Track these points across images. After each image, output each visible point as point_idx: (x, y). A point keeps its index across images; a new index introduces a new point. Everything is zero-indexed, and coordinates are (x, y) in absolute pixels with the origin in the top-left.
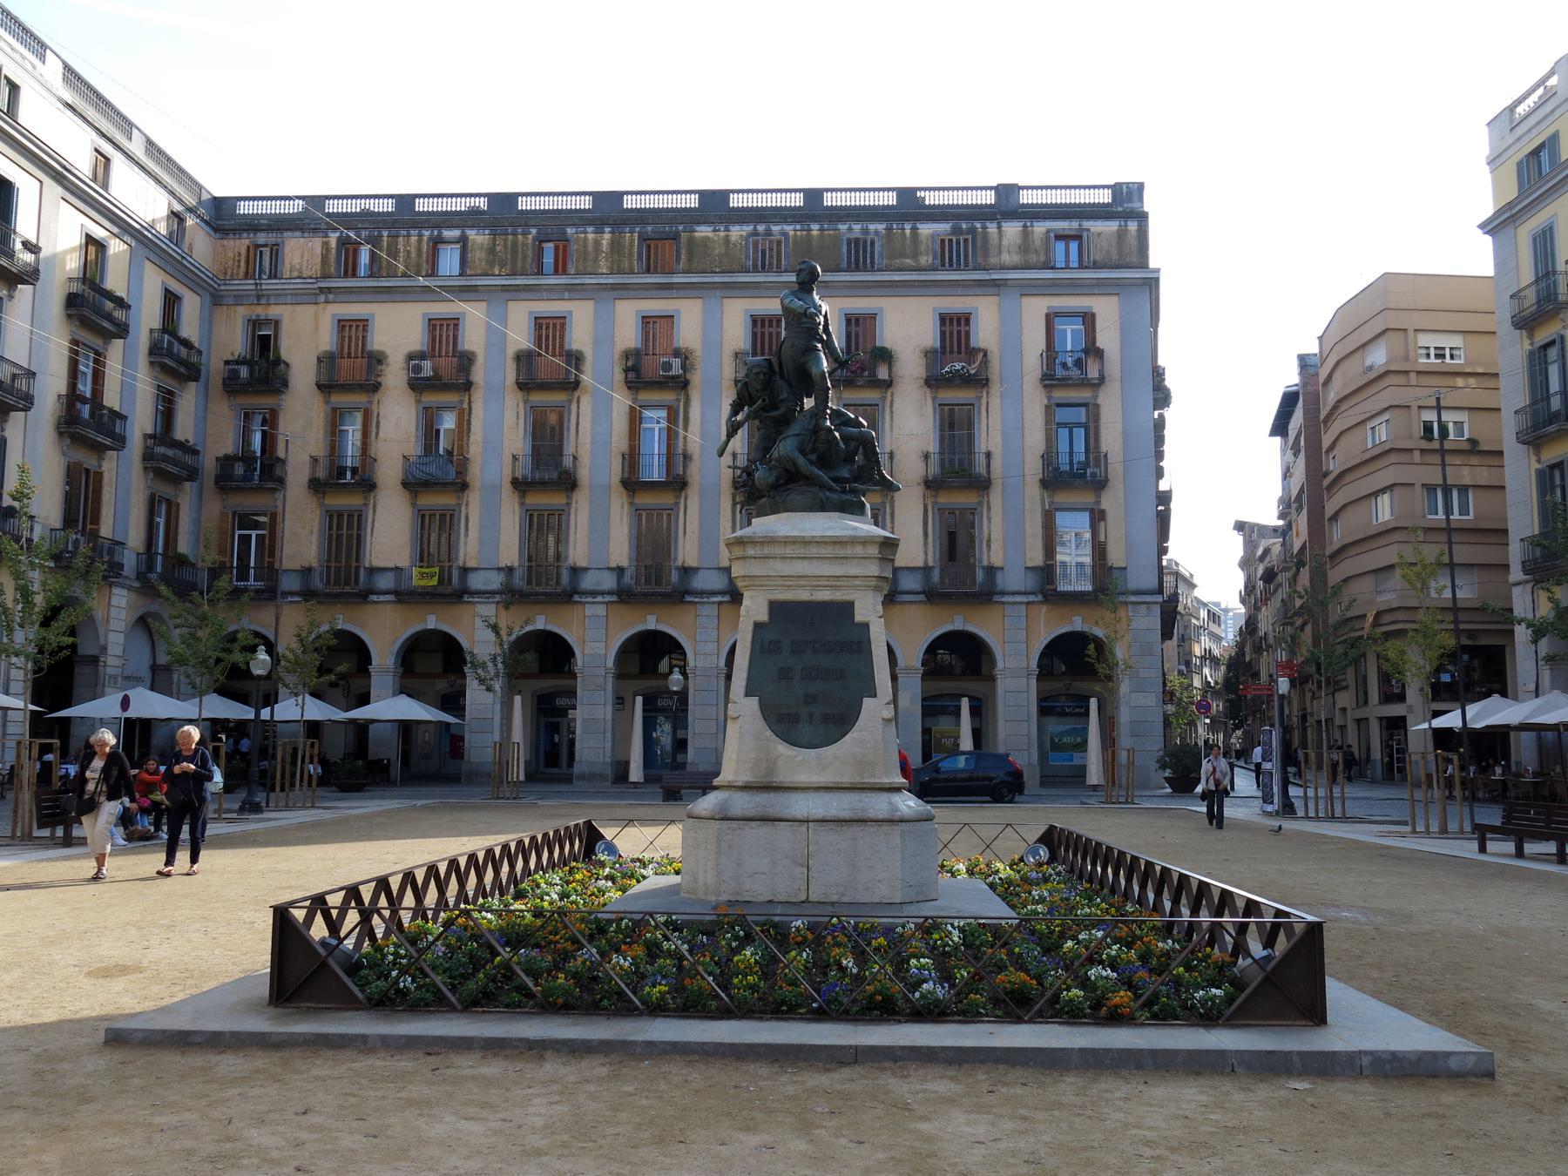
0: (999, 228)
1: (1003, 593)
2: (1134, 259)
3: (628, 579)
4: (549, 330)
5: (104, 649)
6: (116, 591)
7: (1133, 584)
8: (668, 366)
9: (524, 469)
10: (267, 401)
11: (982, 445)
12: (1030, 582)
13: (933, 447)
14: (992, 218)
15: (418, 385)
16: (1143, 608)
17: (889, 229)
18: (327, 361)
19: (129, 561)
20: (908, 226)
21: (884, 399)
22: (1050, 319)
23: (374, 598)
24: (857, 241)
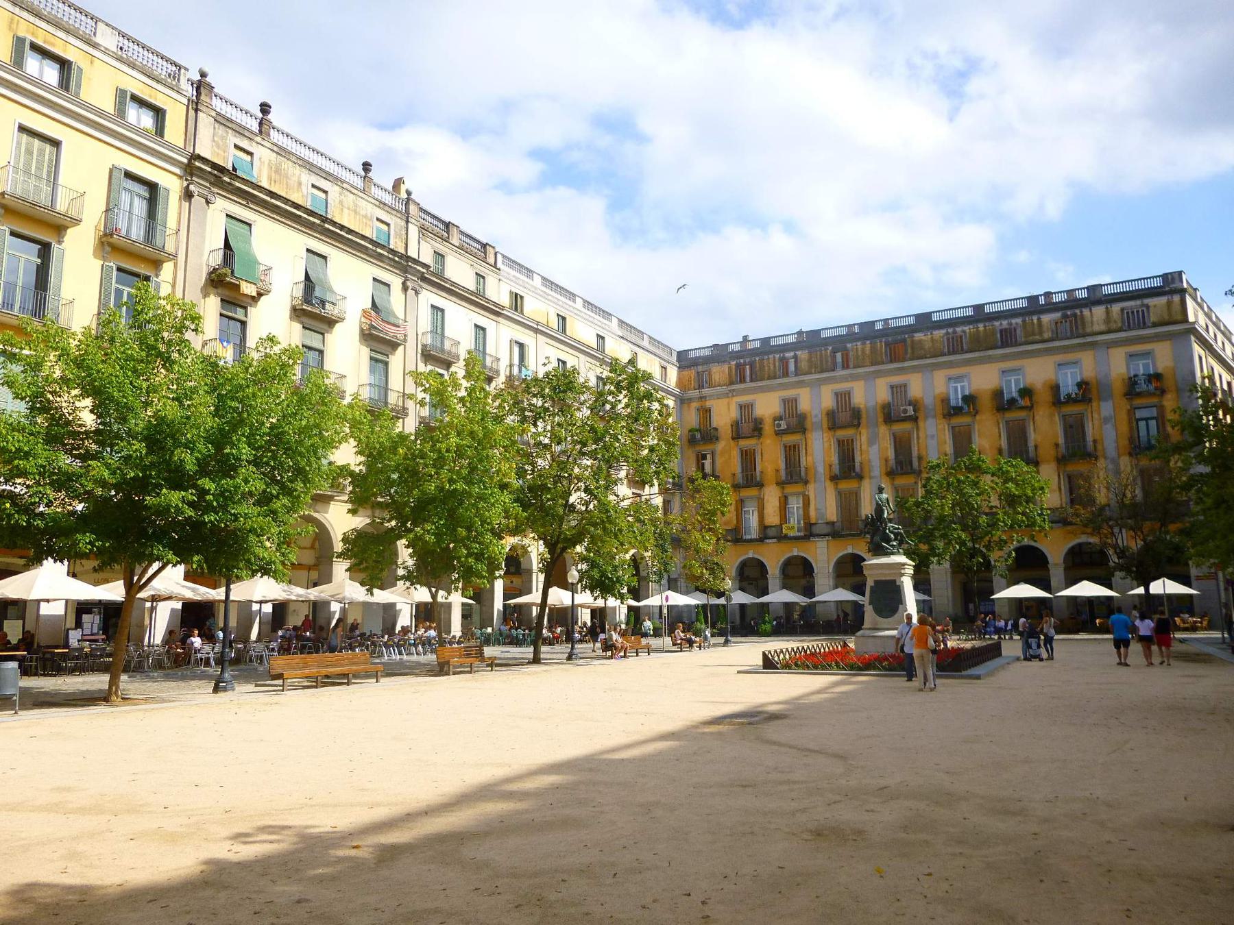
2: (1179, 317)
8: (905, 411)
14: (1086, 306)
17: (1024, 321)
20: (1035, 318)
24: (1006, 329)
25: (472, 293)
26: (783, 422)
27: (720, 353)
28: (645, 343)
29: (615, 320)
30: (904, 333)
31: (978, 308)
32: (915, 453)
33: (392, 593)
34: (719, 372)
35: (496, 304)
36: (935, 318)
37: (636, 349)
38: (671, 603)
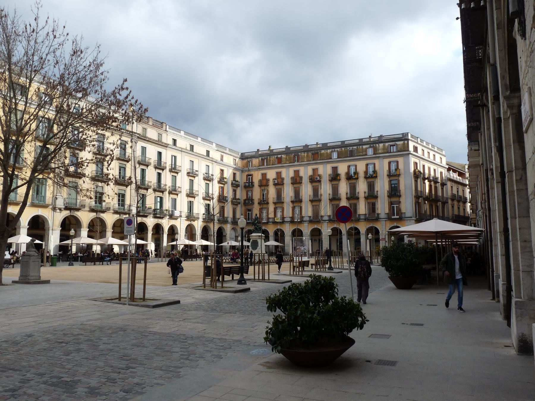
0: (379, 145)
1: (380, 219)
2: (406, 149)
3: (311, 218)
4: (297, 172)
5: (227, 234)
6: (228, 224)
7: (407, 216)
8: (317, 178)
9: (293, 199)
10: (251, 189)
11: (376, 190)
12: (386, 216)
13: (367, 191)
14: (377, 143)
15: (275, 185)
16: (409, 221)
17: (357, 148)
18: (260, 181)
19: (230, 220)
20: (361, 147)
21: (357, 182)
22: (390, 163)
23: (269, 223)
24: (351, 151)
25: (156, 141)
26: (276, 181)
27: (257, 155)
28: (227, 151)
29: (214, 144)
30: (317, 150)
31: (343, 142)
32: (319, 194)
33: (124, 241)
34: (256, 161)
35: (165, 144)
36: (329, 145)
37: (223, 154)
38: (230, 244)
